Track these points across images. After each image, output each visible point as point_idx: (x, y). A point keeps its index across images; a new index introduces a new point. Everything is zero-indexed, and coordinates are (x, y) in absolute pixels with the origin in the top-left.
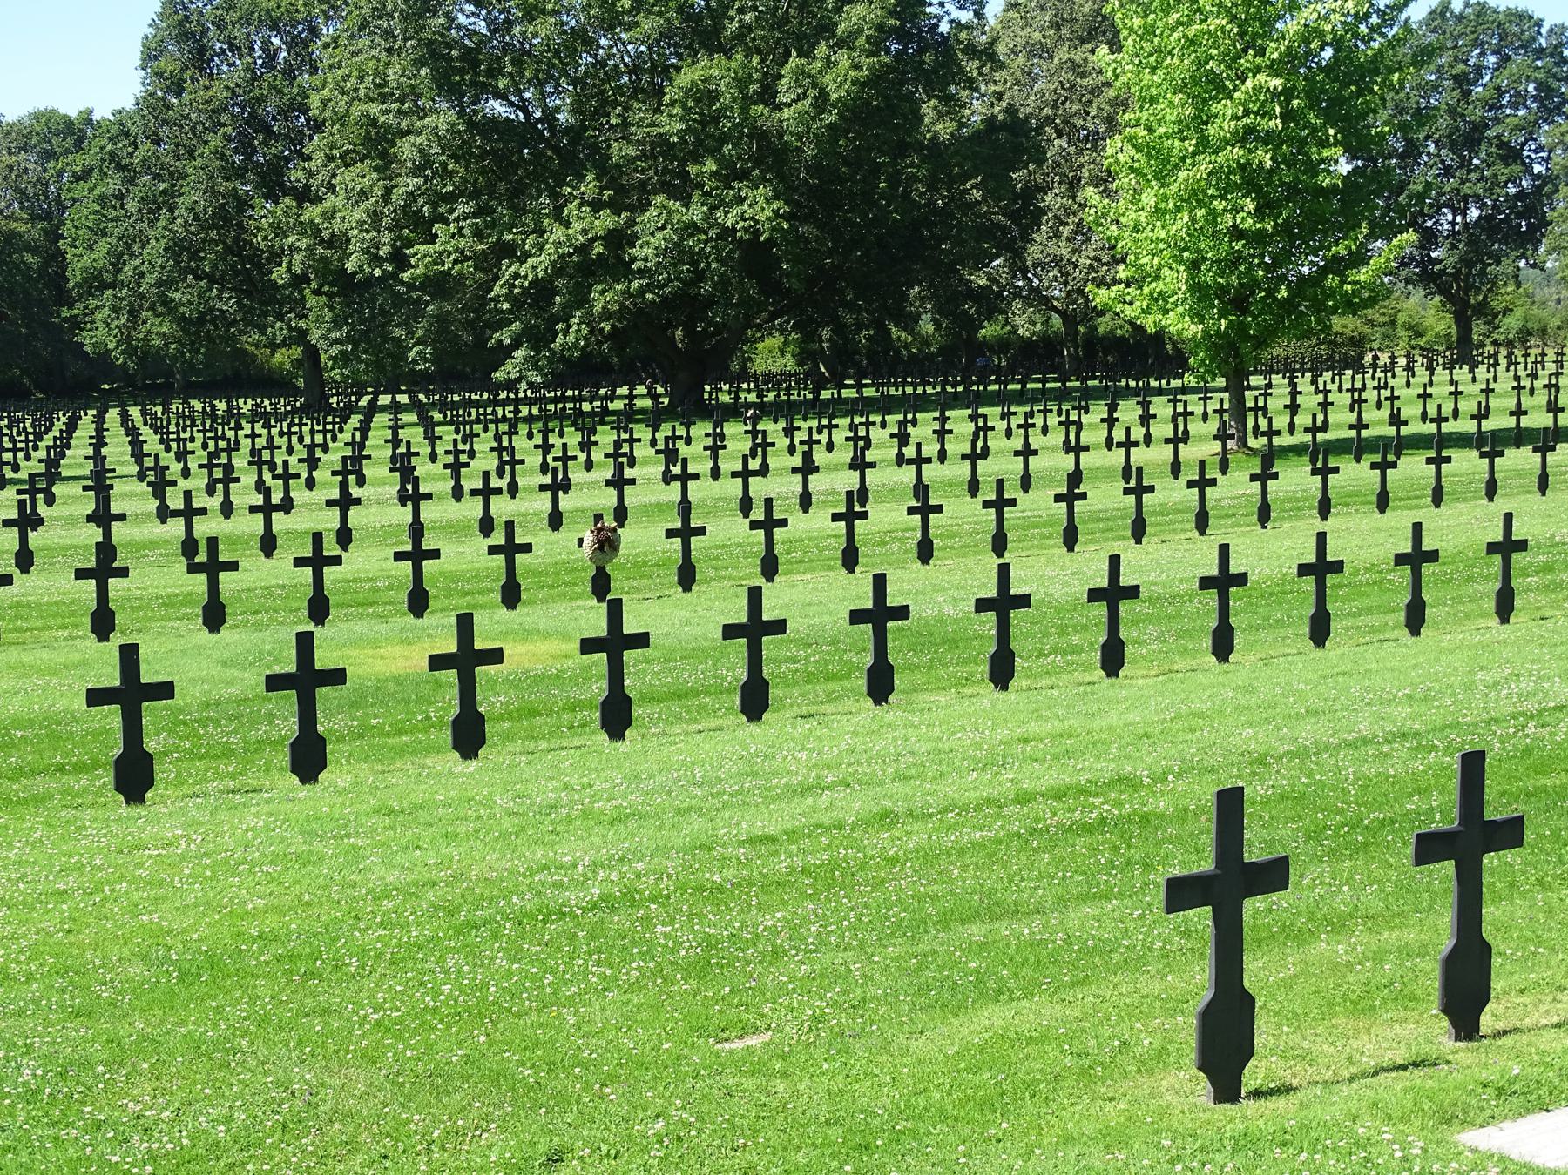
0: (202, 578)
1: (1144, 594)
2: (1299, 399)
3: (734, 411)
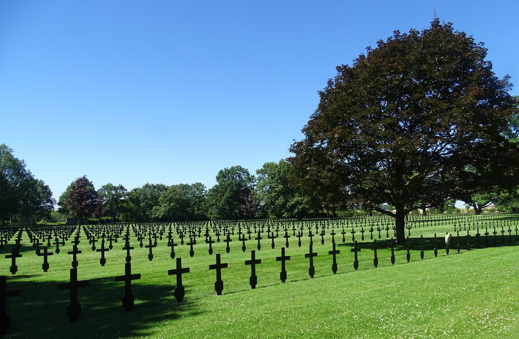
0: (209, 244)
1: (318, 254)
2: (172, 235)
3: (304, 220)
